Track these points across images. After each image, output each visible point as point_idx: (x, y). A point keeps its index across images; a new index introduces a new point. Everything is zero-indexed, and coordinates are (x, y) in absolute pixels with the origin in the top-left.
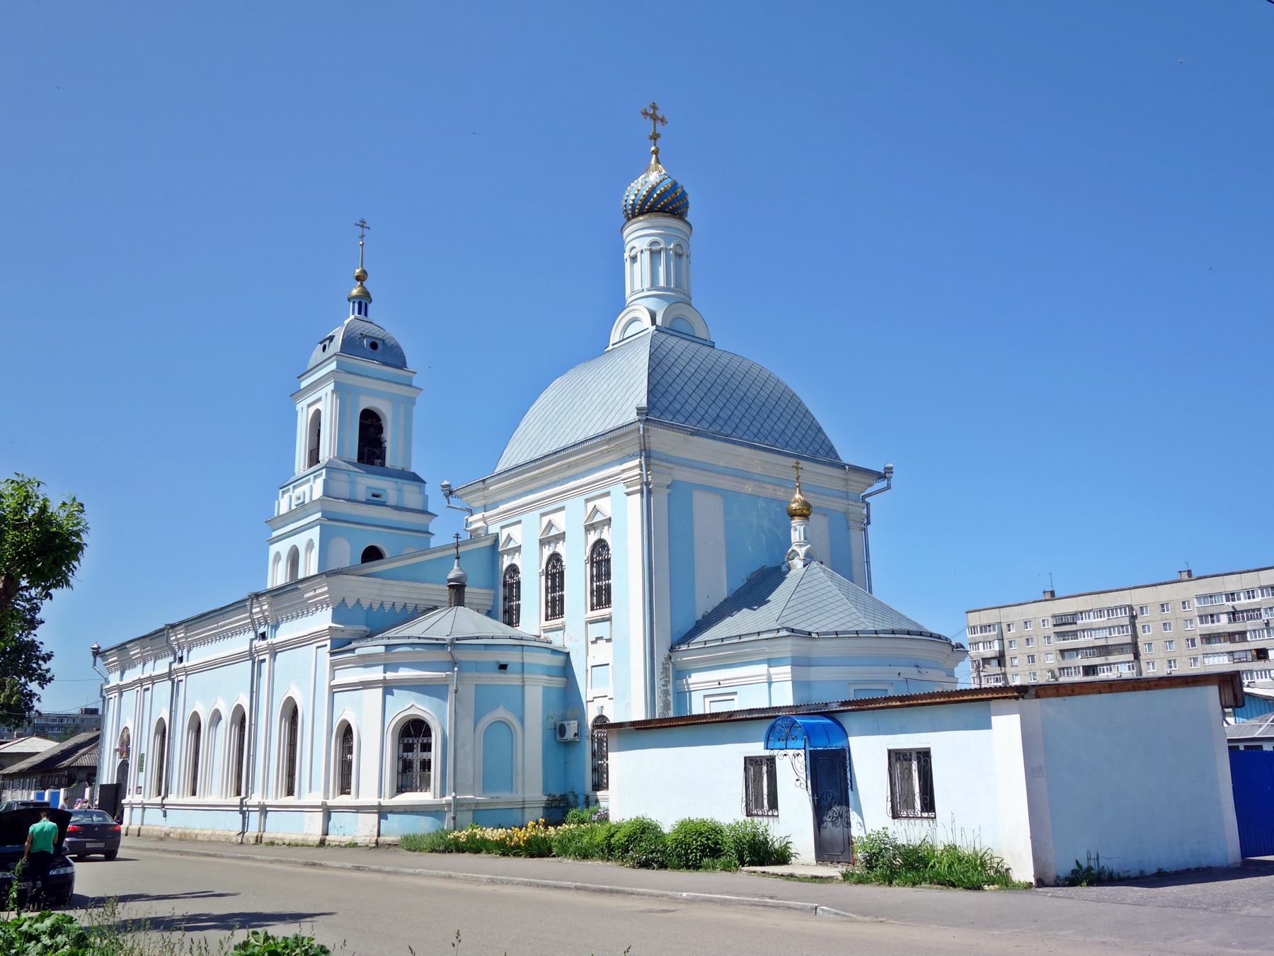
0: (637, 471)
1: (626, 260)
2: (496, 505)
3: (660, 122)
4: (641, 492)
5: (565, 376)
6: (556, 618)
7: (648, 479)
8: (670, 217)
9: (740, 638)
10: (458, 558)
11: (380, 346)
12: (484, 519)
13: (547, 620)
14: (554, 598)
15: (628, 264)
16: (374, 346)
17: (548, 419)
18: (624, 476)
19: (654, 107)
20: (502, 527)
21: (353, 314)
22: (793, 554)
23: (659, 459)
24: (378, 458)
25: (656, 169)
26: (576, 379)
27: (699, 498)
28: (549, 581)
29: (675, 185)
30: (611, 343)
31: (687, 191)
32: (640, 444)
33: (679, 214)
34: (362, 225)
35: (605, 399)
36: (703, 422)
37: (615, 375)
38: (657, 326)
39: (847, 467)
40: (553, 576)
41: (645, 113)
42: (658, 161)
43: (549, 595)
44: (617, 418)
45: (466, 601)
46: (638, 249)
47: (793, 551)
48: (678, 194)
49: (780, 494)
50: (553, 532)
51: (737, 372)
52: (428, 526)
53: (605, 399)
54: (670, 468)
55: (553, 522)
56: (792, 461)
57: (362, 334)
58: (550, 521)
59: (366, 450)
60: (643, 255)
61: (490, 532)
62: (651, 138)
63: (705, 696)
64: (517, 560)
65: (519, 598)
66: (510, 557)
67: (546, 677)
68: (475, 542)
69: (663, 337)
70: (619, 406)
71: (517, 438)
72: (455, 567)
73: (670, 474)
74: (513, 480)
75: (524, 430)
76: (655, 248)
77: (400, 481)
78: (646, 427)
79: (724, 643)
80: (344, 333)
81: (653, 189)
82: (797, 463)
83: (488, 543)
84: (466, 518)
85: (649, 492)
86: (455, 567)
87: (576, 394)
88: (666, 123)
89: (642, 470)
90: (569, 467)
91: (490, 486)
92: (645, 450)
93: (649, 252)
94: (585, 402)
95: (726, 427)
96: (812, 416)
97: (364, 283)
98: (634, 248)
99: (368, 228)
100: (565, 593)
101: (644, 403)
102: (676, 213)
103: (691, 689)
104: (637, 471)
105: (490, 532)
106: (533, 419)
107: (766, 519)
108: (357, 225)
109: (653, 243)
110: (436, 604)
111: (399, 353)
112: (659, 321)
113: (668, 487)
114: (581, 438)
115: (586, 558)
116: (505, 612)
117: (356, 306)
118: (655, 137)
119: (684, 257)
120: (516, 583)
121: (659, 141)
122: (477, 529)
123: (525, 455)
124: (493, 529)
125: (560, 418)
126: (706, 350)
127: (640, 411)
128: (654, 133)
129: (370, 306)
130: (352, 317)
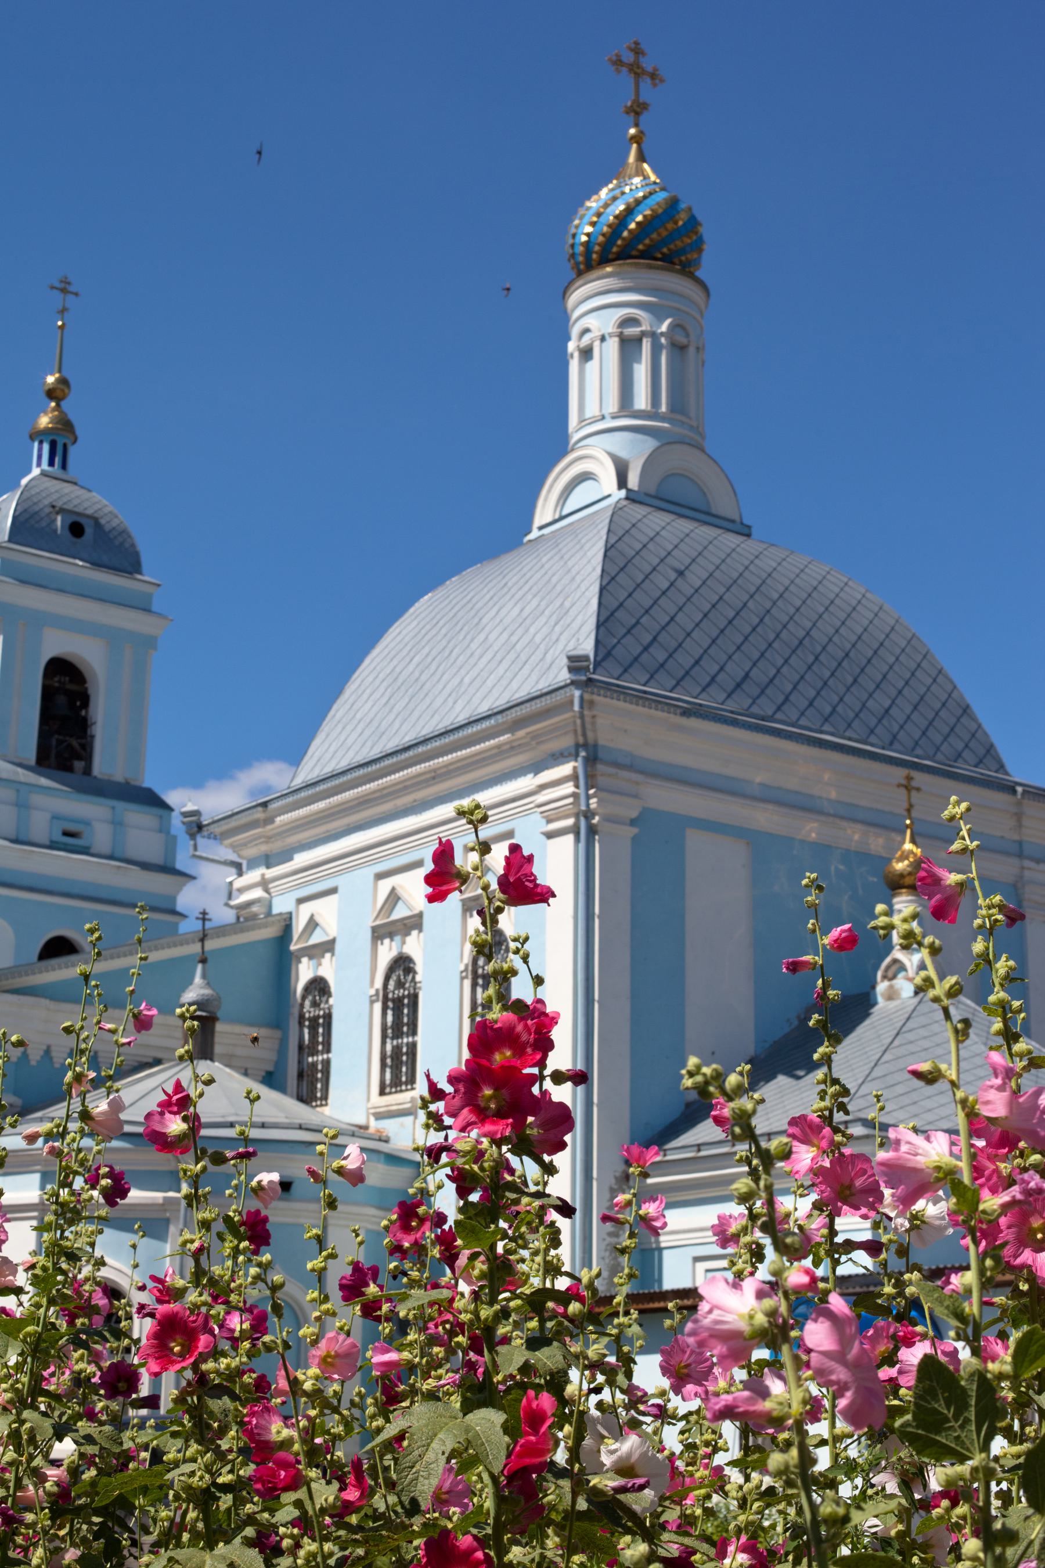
0: (569, 788)
1: (572, 356)
2: (286, 856)
3: (648, 80)
4: (575, 830)
5: (440, 592)
6: (401, 1091)
7: (588, 805)
8: (662, 268)
9: (699, 1150)
10: (203, 961)
11: (89, 531)
12: (264, 884)
13: (382, 1093)
14: (397, 1050)
15: (574, 365)
16: (76, 529)
17: (400, 680)
18: (541, 798)
19: (637, 50)
20: (300, 901)
21: (39, 464)
22: (894, 968)
23: (616, 765)
24: (79, 758)
25: (640, 172)
26: (458, 599)
27: (695, 840)
28: (390, 1013)
29: (673, 203)
30: (538, 521)
31: (700, 217)
32: (575, 731)
33: (681, 263)
34: (64, 288)
35: (514, 639)
36: (713, 690)
37: (535, 590)
38: (629, 491)
39: (1019, 789)
40: (398, 1003)
41: (618, 62)
42: (641, 158)
43: (388, 1041)
44: (534, 678)
45: (218, 1049)
46: (595, 333)
47: (895, 961)
48: (681, 223)
49: (876, 843)
50: (400, 912)
51: (792, 588)
52: (173, 899)
53: (514, 639)
54: (637, 783)
55: (400, 892)
56: (899, 774)
57: (53, 507)
58: (393, 889)
59: (54, 743)
60: (604, 344)
61: (276, 910)
62: (629, 111)
63: (697, 1259)
64: (327, 969)
65: (328, 1049)
66: (313, 962)
67: (373, 1211)
68: (242, 931)
69: (638, 511)
70: (539, 654)
71: (338, 717)
72: (198, 980)
73: (636, 796)
74: (321, 805)
75: (351, 701)
76: (632, 331)
77: (120, 805)
78: (587, 696)
79: (703, 1153)
80: (17, 505)
81: (630, 211)
82: (909, 778)
83: (270, 932)
84: (229, 880)
85: (592, 831)
86: (198, 980)
87: (458, 628)
88: (662, 81)
89: (577, 786)
90: (434, 778)
91: (276, 816)
92: (585, 746)
93: (616, 339)
94: (473, 646)
95: (763, 700)
96: (952, 682)
97: (63, 404)
98: (587, 331)
99: (76, 294)
100: (419, 1039)
101: (587, 647)
102: (676, 260)
103: (663, 1245)
104: (569, 788)
105: (276, 910)
106: (370, 679)
107: (846, 897)
108: (53, 288)
109: (629, 321)
110: (159, 1055)
111: (127, 545)
112: (633, 481)
113: (633, 822)
114: (461, 719)
115: (462, 968)
116: (300, 1075)
117: (46, 447)
118: (637, 110)
119: (692, 350)
120: (324, 1017)
121: (644, 118)
122: (249, 904)
123: (351, 754)
124: (282, 905)
125: (423, 678)
126: (732, 540)
127: (576, 664)
128: (636, 101)
129: (72, 451)
130: (36, 471)
